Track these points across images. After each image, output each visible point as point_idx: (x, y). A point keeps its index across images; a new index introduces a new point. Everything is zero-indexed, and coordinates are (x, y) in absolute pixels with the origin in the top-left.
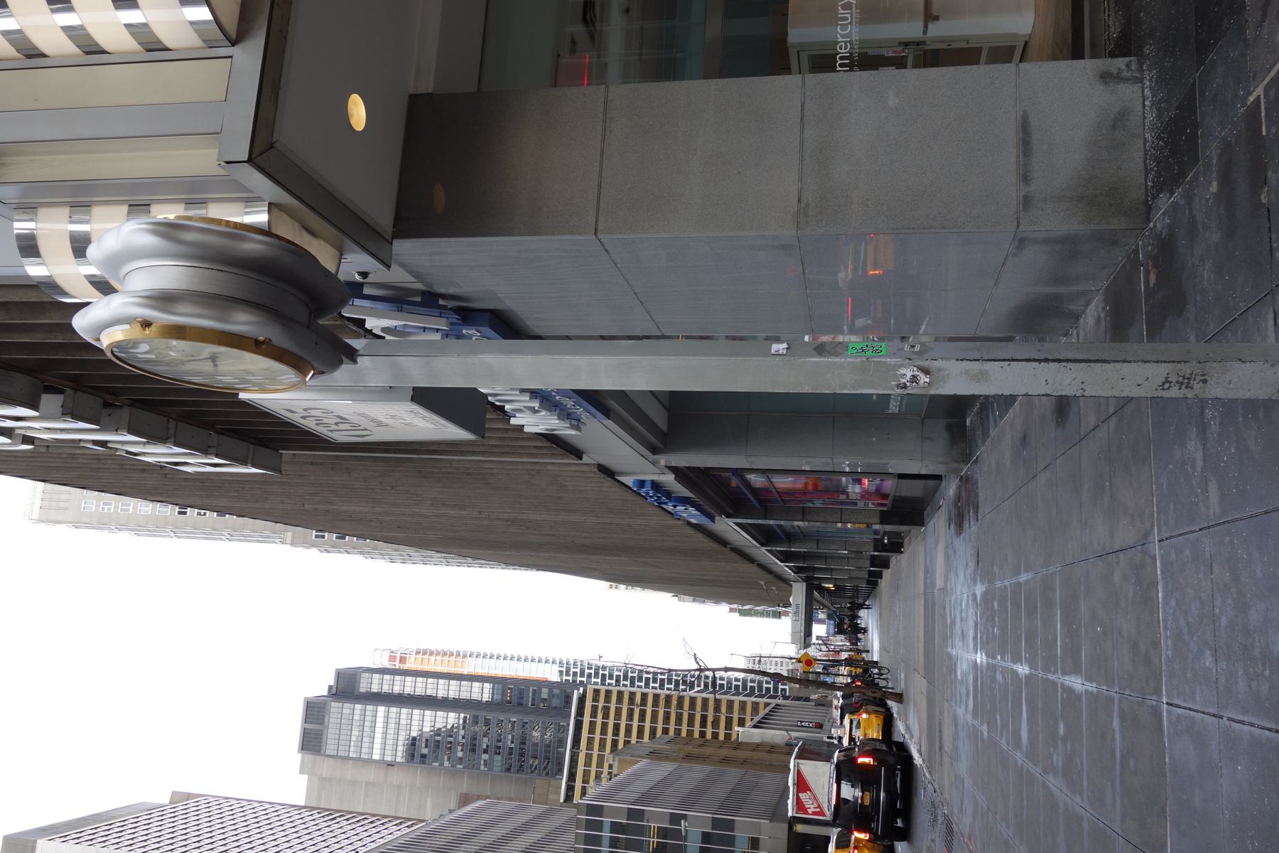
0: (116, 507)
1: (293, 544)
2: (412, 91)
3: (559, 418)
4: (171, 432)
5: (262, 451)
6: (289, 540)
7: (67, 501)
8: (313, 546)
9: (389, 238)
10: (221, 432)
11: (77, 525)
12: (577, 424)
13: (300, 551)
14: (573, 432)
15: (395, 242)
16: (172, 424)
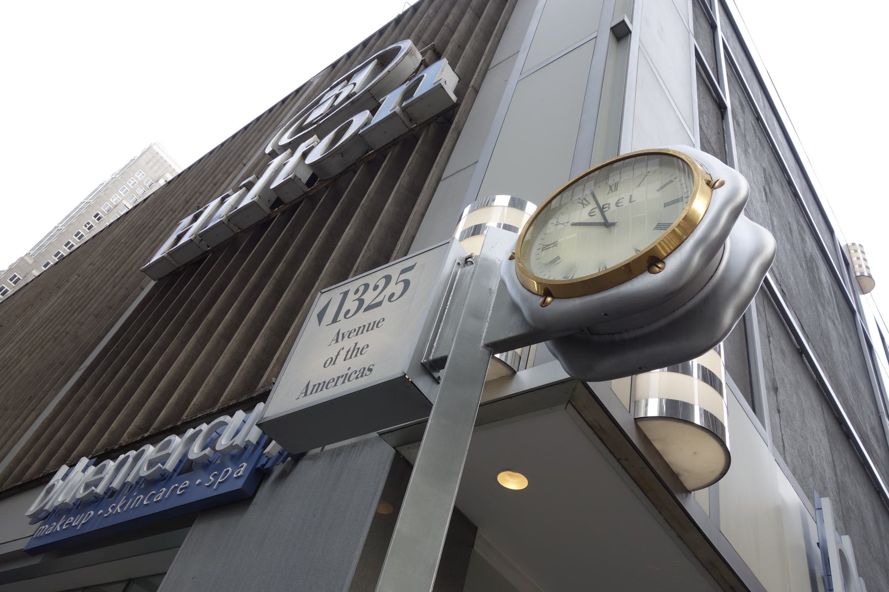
0: (128, 187)
1: (22, 259)
2: (479, 532)
3: (63, 503)
4: (231, 226)
5: (170, 270)
6: (27, 258)
7: (151, 168)
8: (11, 269)
9: (399, 449)
10: (205, 255)
11: (134, 162)
12: (44, 517)
13: (13, 259)
14: (33, 509)
15: (393, 451)
16: (237, 230)
